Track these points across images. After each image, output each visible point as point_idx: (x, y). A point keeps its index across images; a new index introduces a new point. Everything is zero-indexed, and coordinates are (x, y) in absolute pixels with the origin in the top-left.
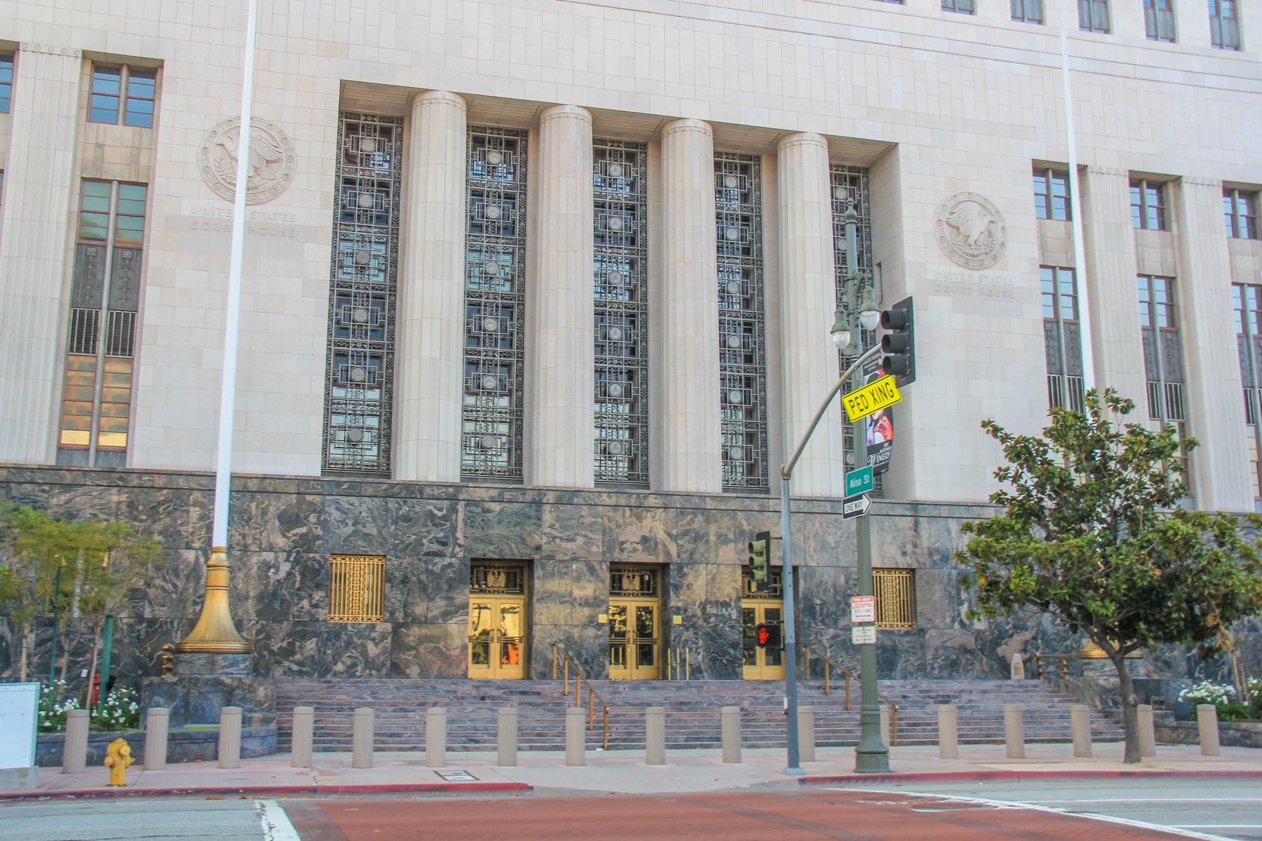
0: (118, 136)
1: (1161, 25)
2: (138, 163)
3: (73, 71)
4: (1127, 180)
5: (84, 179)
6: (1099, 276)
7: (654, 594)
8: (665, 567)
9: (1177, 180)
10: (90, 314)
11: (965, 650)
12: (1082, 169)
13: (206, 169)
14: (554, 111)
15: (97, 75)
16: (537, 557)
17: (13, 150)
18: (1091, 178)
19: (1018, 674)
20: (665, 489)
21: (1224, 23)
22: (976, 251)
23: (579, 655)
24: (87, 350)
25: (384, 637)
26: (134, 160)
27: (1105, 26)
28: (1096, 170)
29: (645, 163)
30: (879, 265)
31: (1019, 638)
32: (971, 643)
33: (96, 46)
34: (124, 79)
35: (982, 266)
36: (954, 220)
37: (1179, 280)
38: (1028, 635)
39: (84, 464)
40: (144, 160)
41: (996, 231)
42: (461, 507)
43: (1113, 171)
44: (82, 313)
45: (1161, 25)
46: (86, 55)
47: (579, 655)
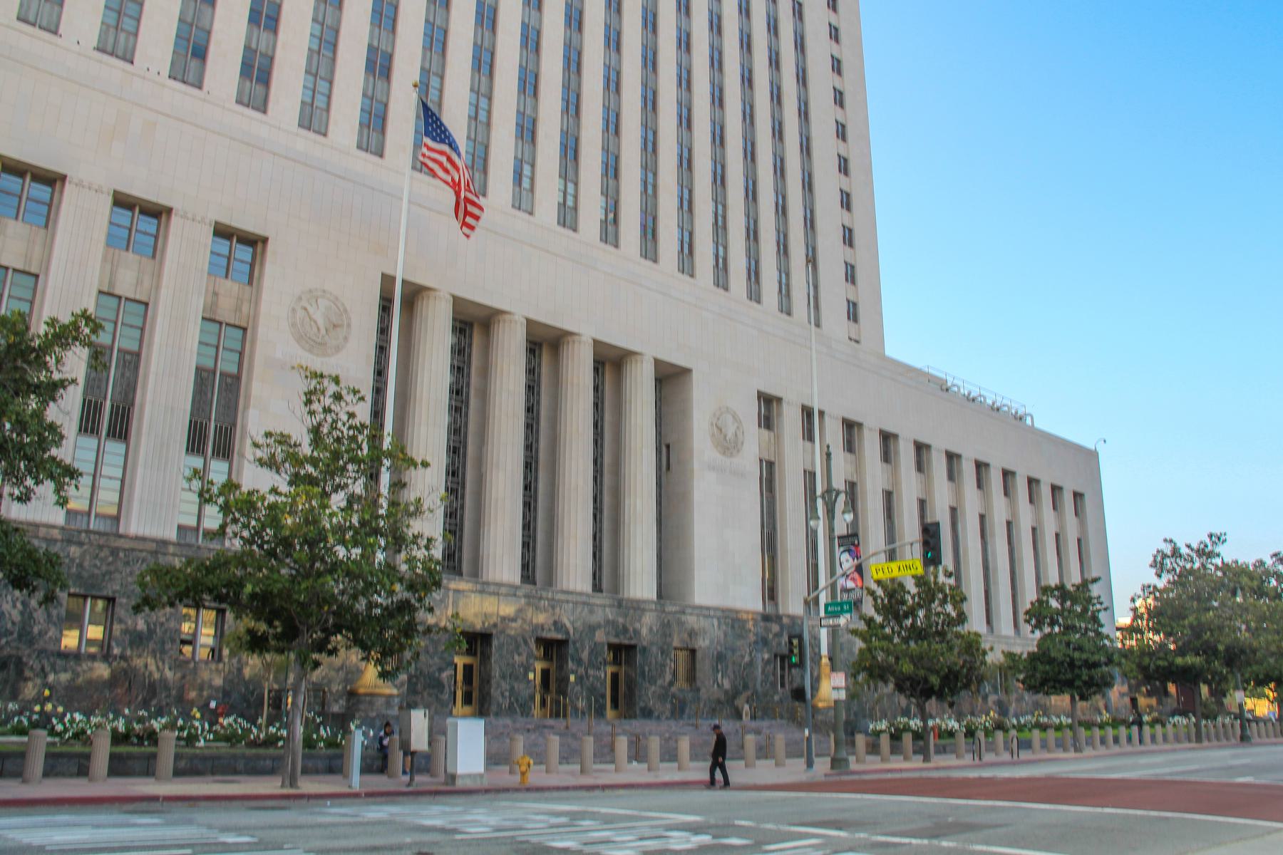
0: (230, 289)
1: (118, 39)
2: (241, 311)
3: (206, 235)
4: (110, 200)
5: (100, 292)
6: (259, 336)
7: (475, 654)
8: (631, 648)
9: (779, 400)
10: (96, 403)
11: (719, 702)
12: (821, 413)
13: (294, 325)
14: (507, 317)
15: (116, 209)
16: (494, 632)
17: (163, 291)
18: (826, 418)
19: (746, 718)
20: (565, 588)
21: (524, 193)
22: (729, 446)
23: (517, 700)
24: (92, 432)
25: (402, 684)
26: (238, 309)
27: (53, 28)
28: (75, 180)
29: (471, 337)
30: (668, 447)
31: (743, 697)
32: (722, 698)
33: (226, 220)
34: (242, 244)
35: (732, 455)
36: (719, 423)
37: (249, 331)
38: (749, 693)
39: (193, 541)
40: (245, 309)
41: (740, 436)
42: (451, 594)
43: (199, 218)
44: (90, 402)
45: (118, 39)
46: (116, 193)
47: (517, 700)
